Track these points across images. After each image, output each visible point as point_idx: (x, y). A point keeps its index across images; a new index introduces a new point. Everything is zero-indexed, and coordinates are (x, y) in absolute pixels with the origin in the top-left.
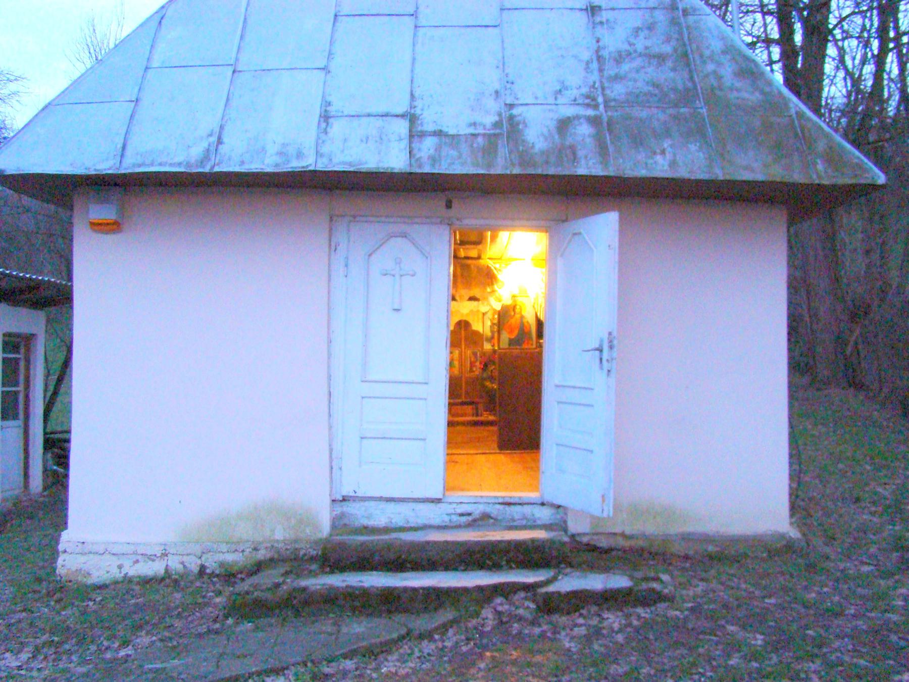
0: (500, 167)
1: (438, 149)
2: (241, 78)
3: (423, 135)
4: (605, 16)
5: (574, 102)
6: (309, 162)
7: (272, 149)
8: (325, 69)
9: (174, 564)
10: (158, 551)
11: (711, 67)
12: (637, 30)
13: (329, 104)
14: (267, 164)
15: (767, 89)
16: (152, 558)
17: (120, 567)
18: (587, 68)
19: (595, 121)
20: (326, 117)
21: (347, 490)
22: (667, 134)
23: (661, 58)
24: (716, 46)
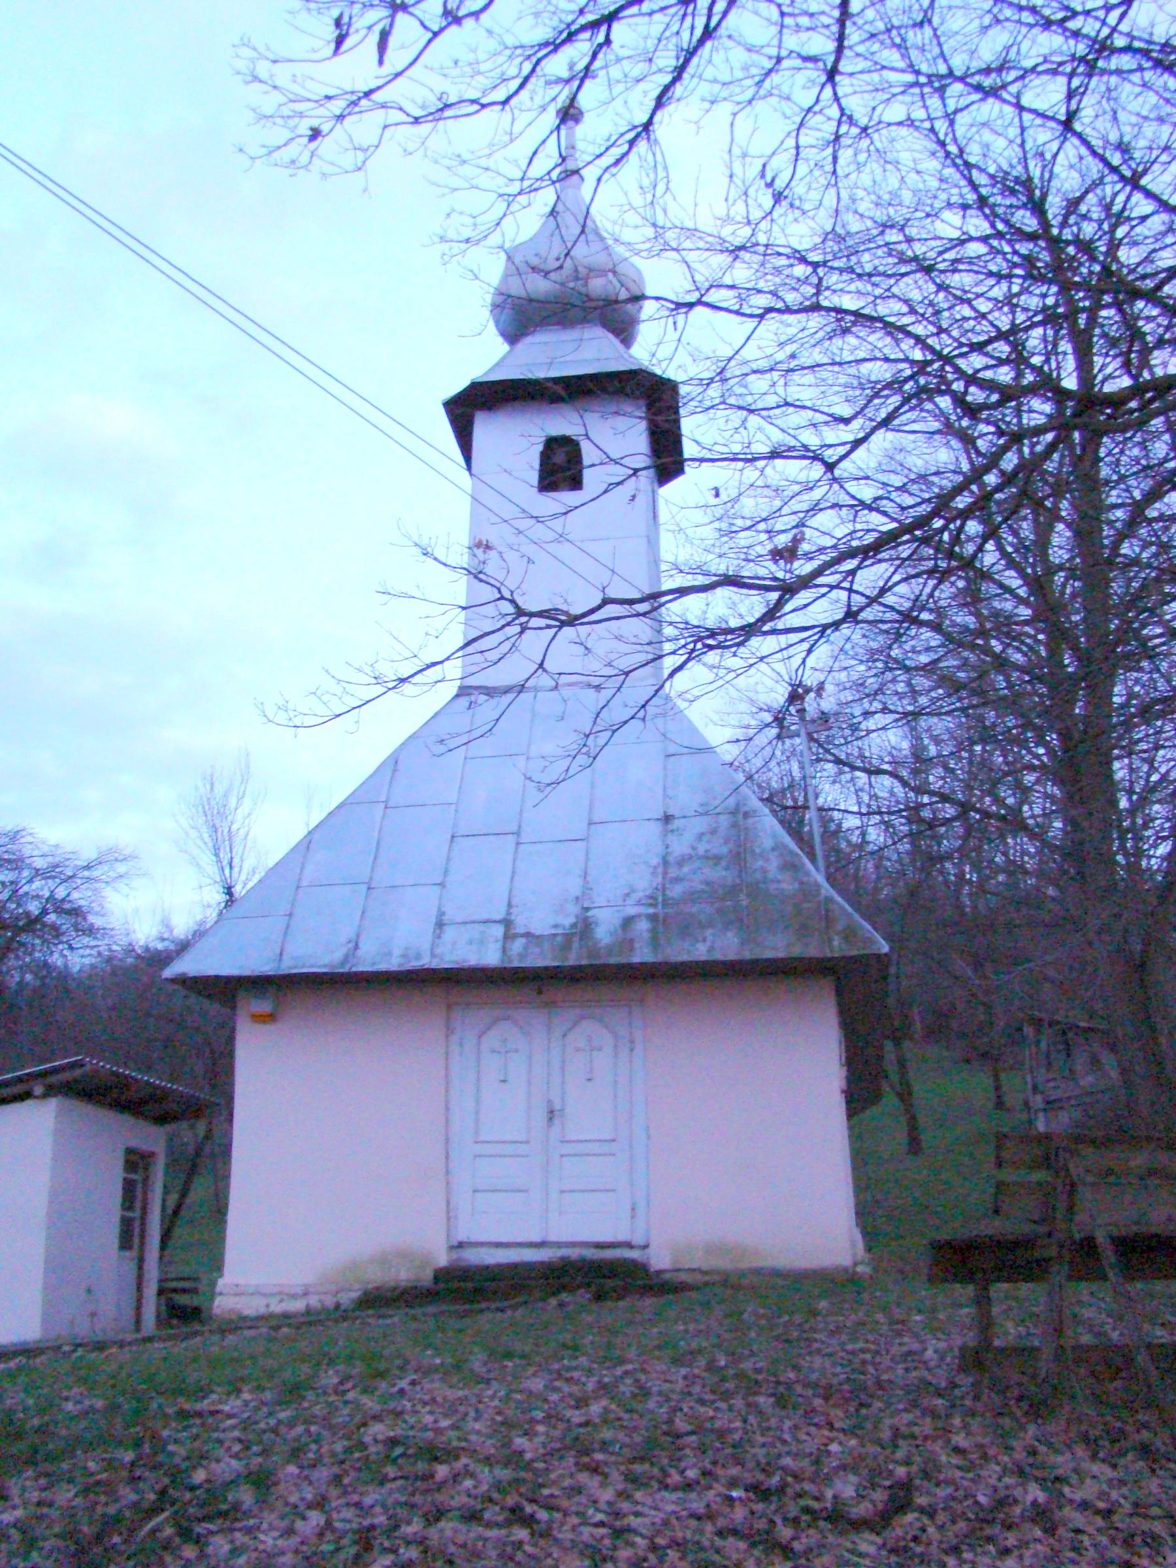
0: (572, 960)
1: (526, 947)
2: (375, 893)
3: (516, 936)
4: (676, 824)
5: (639, 903)
6: (426, 962)
7: (397, 952)
8: (442, 885)
9: (314, 1301)
10: (299, 1290)
11: (760, 863)
12: (701, 836)
13: (443, 914)
14: (393, 964)
15: (805, 879)
16: (294, 1296)
17: (268, 1306)
18: (654, 873)
19: (653, 918)
20: (440, 925)
21: (462, 1236)
22: (710, 924)
23: (717, 859)
24: (768, 843)
